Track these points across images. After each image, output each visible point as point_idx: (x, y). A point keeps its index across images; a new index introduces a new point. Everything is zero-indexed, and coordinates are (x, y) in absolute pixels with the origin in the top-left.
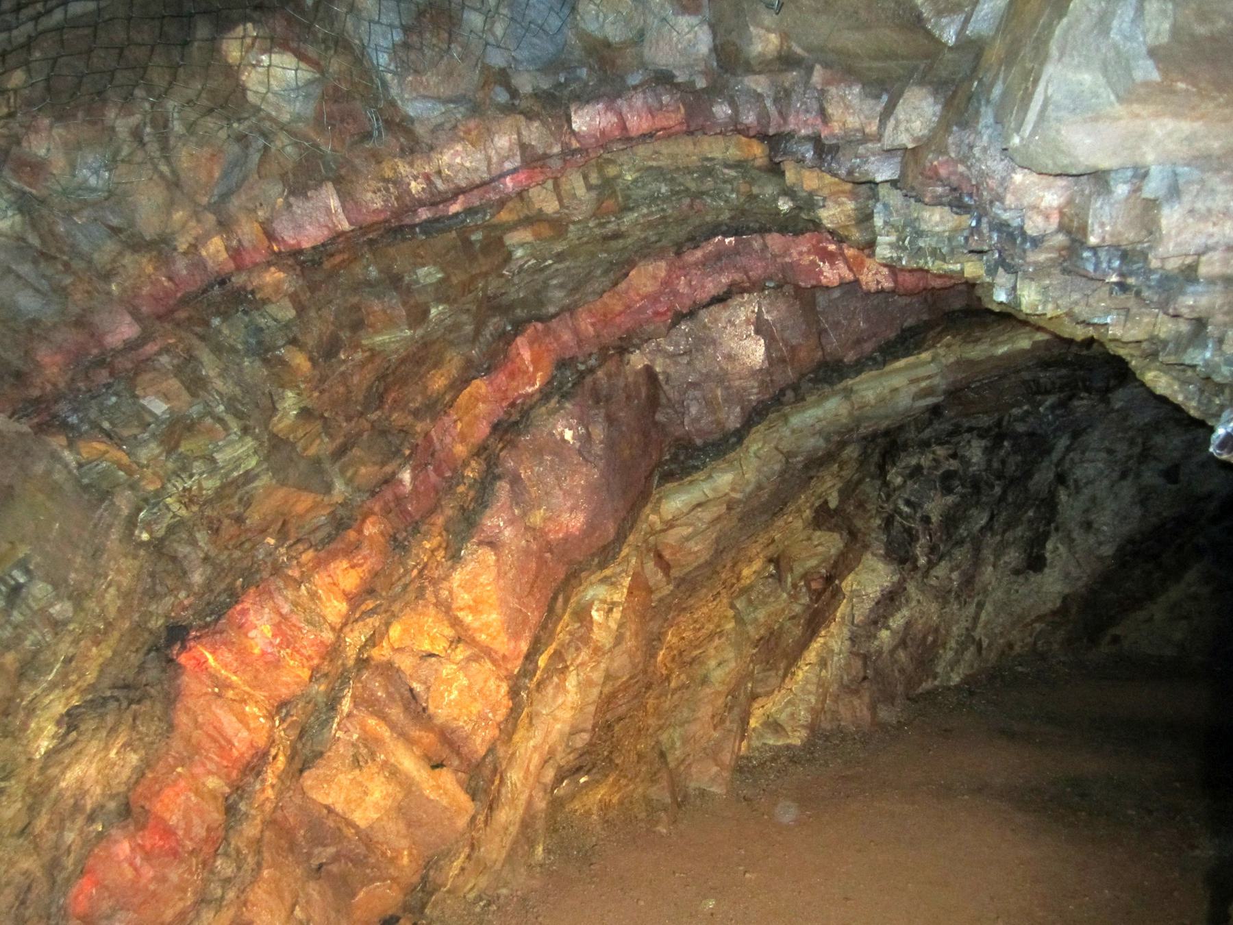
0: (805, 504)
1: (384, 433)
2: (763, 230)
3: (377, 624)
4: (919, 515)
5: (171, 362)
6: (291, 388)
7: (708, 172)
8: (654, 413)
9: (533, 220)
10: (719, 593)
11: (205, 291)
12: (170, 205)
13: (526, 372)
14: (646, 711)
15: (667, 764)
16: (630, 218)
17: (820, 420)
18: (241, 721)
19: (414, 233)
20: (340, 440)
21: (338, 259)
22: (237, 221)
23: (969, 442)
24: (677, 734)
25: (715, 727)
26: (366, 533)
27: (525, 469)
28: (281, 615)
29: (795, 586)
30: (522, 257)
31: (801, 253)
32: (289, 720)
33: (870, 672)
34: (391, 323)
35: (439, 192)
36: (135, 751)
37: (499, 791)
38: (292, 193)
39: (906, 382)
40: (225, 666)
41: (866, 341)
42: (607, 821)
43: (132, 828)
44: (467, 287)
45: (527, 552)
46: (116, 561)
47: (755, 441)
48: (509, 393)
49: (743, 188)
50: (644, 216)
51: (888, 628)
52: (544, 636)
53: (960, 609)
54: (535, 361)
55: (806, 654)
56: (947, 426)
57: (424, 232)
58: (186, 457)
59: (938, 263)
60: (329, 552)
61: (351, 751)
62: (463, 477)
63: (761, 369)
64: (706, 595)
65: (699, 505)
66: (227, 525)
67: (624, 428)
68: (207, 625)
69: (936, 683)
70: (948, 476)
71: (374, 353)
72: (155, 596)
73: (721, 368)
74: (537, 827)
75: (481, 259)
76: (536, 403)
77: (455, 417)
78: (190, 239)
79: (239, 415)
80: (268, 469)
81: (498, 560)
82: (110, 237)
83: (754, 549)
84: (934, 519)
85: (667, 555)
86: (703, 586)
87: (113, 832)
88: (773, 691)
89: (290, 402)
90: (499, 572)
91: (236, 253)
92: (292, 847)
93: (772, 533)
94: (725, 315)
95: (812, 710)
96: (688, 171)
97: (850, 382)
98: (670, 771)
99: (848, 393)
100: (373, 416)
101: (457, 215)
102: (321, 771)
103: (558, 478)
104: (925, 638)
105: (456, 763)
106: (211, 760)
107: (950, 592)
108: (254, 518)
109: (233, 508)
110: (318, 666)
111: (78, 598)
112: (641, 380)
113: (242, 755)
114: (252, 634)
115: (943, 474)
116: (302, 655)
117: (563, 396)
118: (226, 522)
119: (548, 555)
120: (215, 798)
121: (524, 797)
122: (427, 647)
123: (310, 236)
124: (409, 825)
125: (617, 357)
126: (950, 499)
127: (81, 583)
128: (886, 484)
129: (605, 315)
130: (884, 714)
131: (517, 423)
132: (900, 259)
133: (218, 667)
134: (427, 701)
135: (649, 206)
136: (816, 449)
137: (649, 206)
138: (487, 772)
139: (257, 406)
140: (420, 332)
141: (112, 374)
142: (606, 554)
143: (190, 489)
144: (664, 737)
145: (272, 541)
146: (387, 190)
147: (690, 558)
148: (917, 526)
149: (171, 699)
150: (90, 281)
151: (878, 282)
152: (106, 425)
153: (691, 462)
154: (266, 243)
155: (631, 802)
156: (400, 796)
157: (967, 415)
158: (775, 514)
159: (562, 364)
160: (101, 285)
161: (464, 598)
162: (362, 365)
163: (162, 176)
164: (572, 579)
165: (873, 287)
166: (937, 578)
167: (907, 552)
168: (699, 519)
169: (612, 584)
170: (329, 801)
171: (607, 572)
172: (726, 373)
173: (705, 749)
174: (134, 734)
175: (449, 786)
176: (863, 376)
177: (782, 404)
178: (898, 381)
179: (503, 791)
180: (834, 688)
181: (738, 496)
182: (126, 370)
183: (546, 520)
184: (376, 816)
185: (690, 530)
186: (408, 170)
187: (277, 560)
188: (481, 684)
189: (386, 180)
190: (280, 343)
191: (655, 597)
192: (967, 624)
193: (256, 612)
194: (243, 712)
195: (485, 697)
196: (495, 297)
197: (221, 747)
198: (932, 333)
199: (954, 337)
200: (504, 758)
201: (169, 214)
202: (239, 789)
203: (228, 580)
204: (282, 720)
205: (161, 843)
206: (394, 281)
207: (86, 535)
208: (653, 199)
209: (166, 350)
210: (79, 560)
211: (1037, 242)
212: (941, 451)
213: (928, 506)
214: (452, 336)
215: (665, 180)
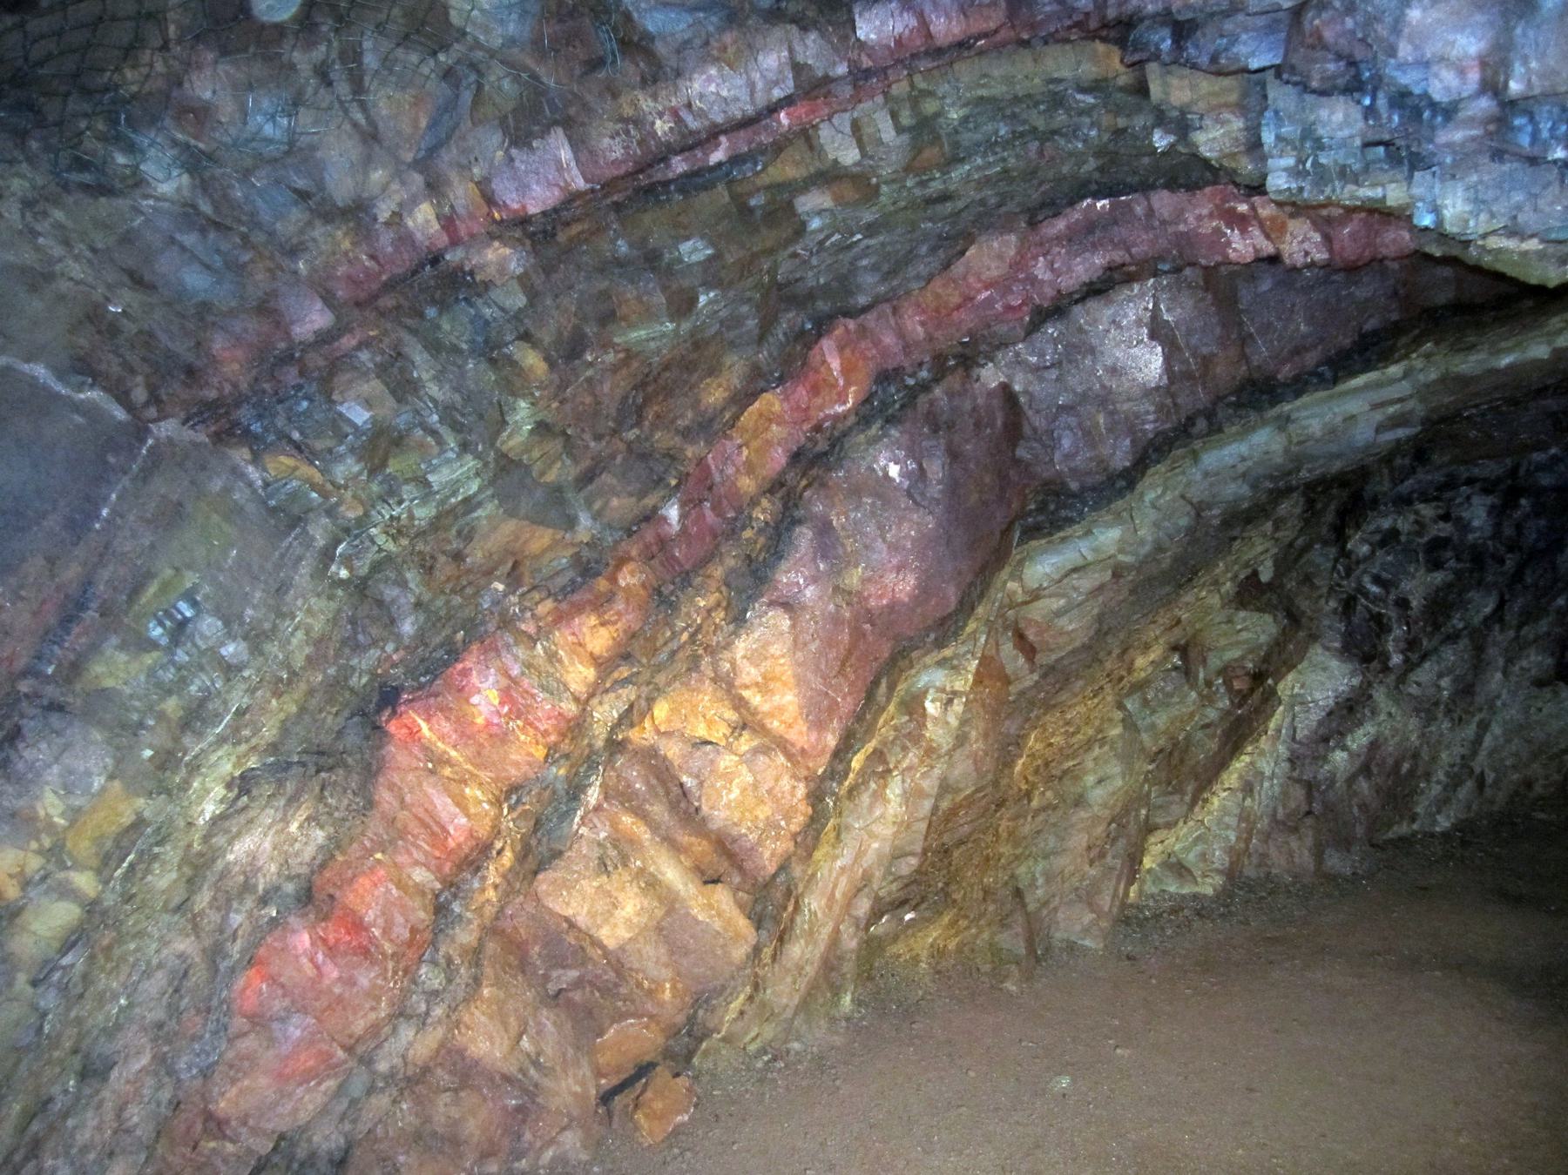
0: (1226, 572)
1: (644, 457)
2: (1145, 187)
3: (633, 697)
4: (1392, 597)
5: (372, 360)
6: (524, 396)
7: (1057, 101)
8: (1014, 446)
9: (830, 176)
10: (1102, 688)
11: (415, 272)
12: (367, 162)
13: (834, 386)
14: (997, 835)
15: (1024, 906)
16: (957, 173)
17: (1244, 459)
18: (458, 804)
19: (668, 193)
20: (586, 463)
21: (576, 229)
22: (448, 183)
23: (1468, 498)
24: (1040, 866)
25: (1091, 863)
26: (622, 583)
27: (838, 515)
28: (509, 677)
29: (1209, 684)
30: (821, 230)
31: (1199, 218)
32: (520, 809)
33: (1317, 807)
34: (649, 315)
35: (691, 133)
36: (322, 827)
37: (792, 920)
38: (515, 143)
39: (1367, 407)
40: (442, 738)
41: (1307, 350)
42: (938, 972)
43: (312, 916)
44: (746, 267)
45: (836, 620)
46: (306, 600)
47: (1153, 486)
48: (812, 413)
49: (1106, 120)
50: (979, 168)
51: (1344, 748)
52: (860, 730)
53: (1451, 729)
54: (847, 371)
55: (1225, 776)
56: (1439, 477)
57: (681, 190)
58: (395, 478)
59: (1350, 187)
60: (573, 604)
61: (596, 853)
62: (750, 518)
63: (1158, 388)
64: (1083, 689)
65: (1075, 570)
66: (444, 568)
67: (972, 466)
68: (421, 687)
69: (1415, 827)
70: (1438, 544)
71: (630, 355)
72: (358, 648)
73: (1103, 386)
74: (845, 970)
75: (764, 231)
76: (850, 429)
77: (739, 441)
78: (394, 207)
79: (457, 428)
80: (493, 496)
81: (793, 626)
82: (296, 203)
83: (1153, 632)
84: (1414, 604)
85: (1031, 635)
86: (1078, 677)
87: (292, 919)
88: (1176, 823)
89: (523, 414)
90: (795, 641)
91: (448, 222)
92: (524, 966)
93: (1177, 612)
94: (1108, 312)
95: (1230, 850)
96: (1030, 100)
97: (1287, 407)
98: (1027, 914)
99: (1284, 422)
100: (632, 435)
101: (720, 164)
102: (559, 874)
103: (881, 527)
104: (1397, 765)
105: (737, 879)
106: (418, 847)
107: (1436, 704)
108: (476, 556)
109: (449, 542)
110: (556, 744)
111: (256, 639)
112: (995, 402)
113: (459, 845)
114: (475, 699)
115: (1429, 542)
116: (536, 728)
117: (887, 421)
118: (442, 559)
119: (867, 626)
120: (423, 894)
121: (825, 932)
122: (701, 731)
123: (538, 199)
124: (672, 953)
125: (960, 371)
126: (1438, 577)
127: (260, 621)
128: (1344, 553)
129: (937, 310)
130: (1335, 861)
131: (825, 454)
132: (1301, 189)
133: (434, 738)
134: (699, 799)
135: (985, 155)
136: (1238, 499)
137: (985, 155)
138: (778, 895)
139: (481, 417)
140: (686, 326)
141: (302, 374)
142: (946, 628)
143: (398, 519)
144: (1021, 870)
145: (501, 587)
146: (627, 132)
147: (1061, 640)
148: (1391, 613)
149: (371, 771)
150: (272, 258)
151: (1307, 254)
152: (296, 435)
153: (1063, 513)
154: (485, 209)
155: (973, 951)
156: (659, 913)
157: (1466, 462)
158: (1180, 586)
159: (885, 377)
160: (286, 262)
161: (749, 673)
162: (615, 369)
163: (355, 125)
164: (898, 662)
165: (1299, 260)
166: (1419, 684)
167: (1374, 646)
168: (1075, 589)
169: (953, 668)
170: (569, 912)
171: (947, 652)
172: (1110, 391)
173: (1077, 889)
174: (321, 806)
175: (724, 907)
176: (1305, 399)
177: (1189, 436)
178: (1355, 406)
179: (798, 919)
180: (1262, 825)
181: (1127, 559)
182: (319, 369)
183: (865, 581)
184: (628, 935)
185: (1062, 602)
186: (652, 104)
187: (507, 610)
188: (771, 784)
189: (624, 120)
190: (508, 338)
191: (1013, 689)
192: (1462, 751)
193: (479, 673)
194: (463, 796)
195: (776, 800)
196: (788, 283)
197: (433, 834)
198: (1404, 340)
199: (1437, 343)
200: (801, 879)
201: (366, 174)
202: (452, 885)
203: (447, 632)
204: (511, 809)
205: (348, 938)
206: (652, 259)
207: (269, 566)
208: (990, 145)
209: (364, 344)
210: (258, 595)
211: (1449, 112)
212: (1427, 511)
213: (1406, 585)
214: (731, 335)
215: (1004, 117)
